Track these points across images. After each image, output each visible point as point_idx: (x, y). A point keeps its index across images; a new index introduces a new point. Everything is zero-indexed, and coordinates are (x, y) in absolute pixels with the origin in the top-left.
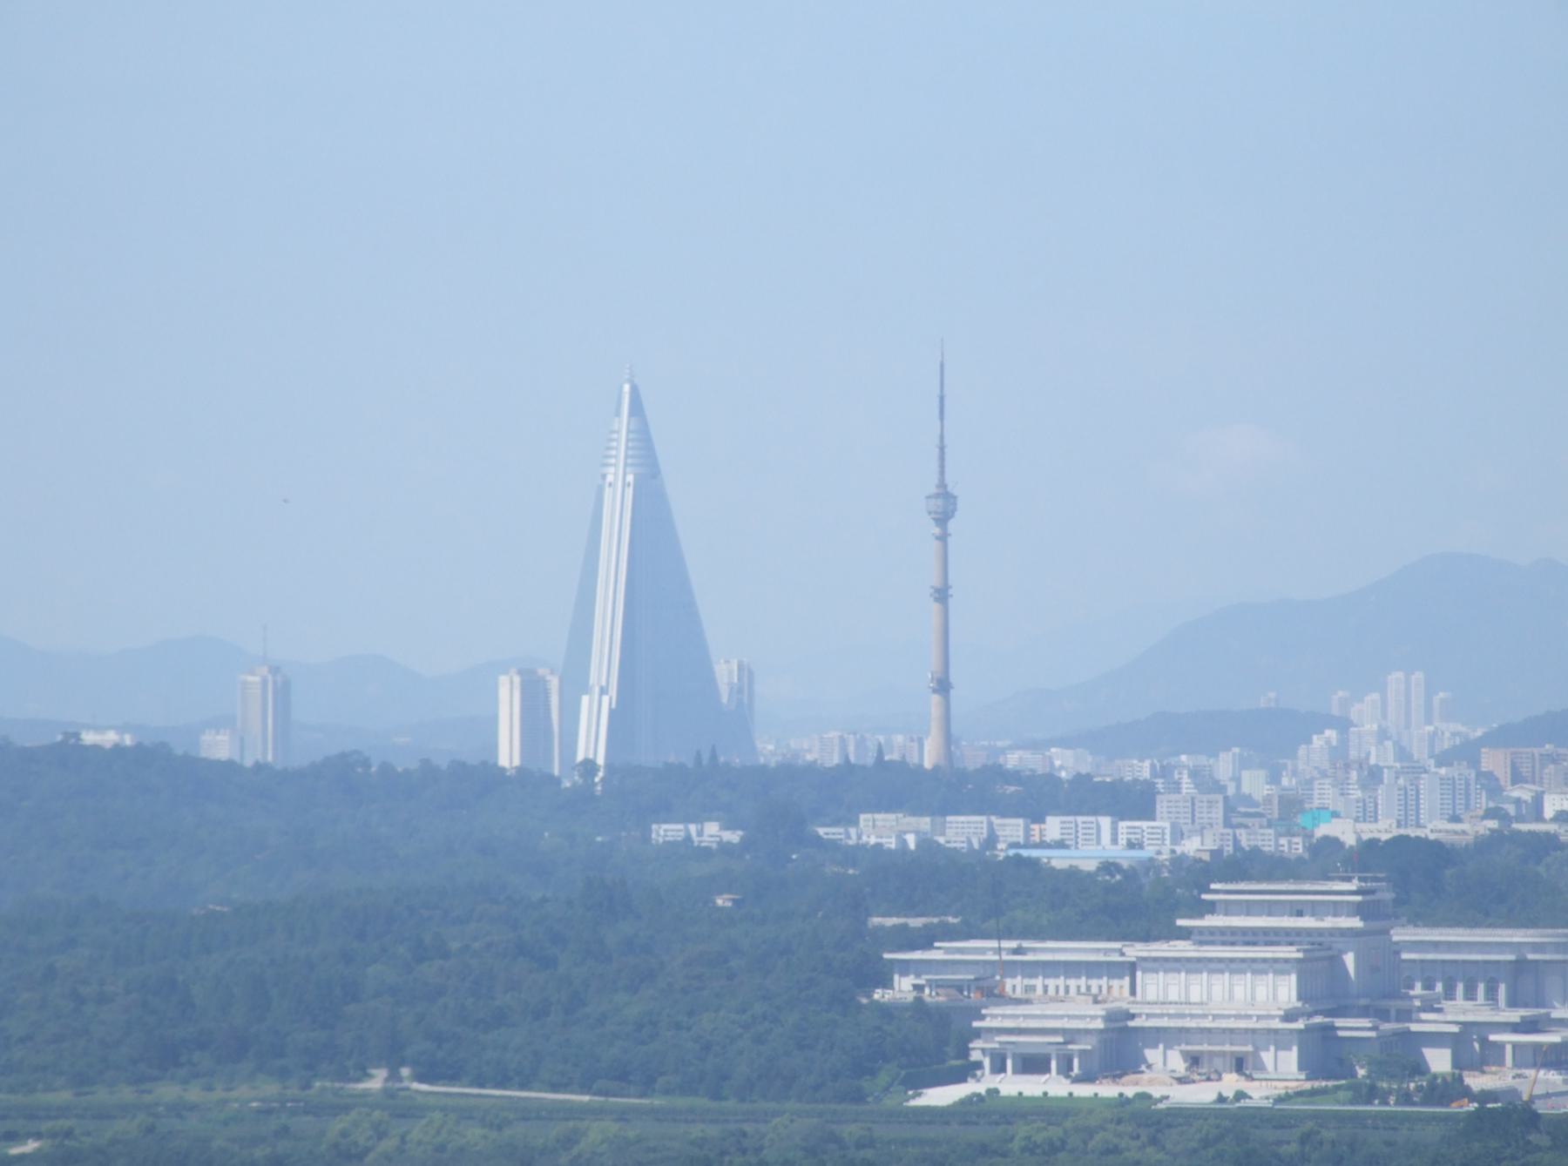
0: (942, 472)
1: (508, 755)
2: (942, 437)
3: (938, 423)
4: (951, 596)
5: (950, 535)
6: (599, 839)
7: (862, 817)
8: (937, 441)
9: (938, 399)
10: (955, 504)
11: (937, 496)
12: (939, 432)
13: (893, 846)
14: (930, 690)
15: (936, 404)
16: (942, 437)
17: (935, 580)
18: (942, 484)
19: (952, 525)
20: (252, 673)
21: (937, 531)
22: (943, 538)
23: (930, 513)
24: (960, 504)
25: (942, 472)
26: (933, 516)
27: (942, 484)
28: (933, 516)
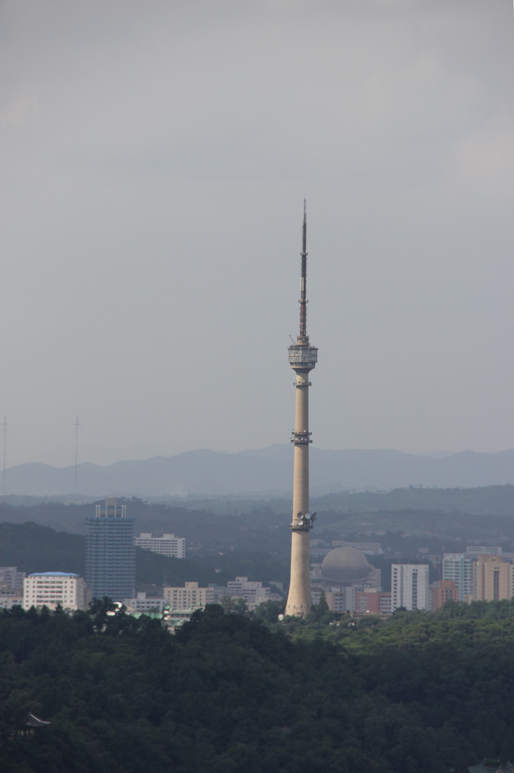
0: (304, 327)
1: (409, 607)
2: (304, 292)
3: (301, 279)
4: (311, 442)
5: (311, 384)
6: (368, 611)
7: (166, 590)
8: (299, 297)
9: (300, 258)
10: (316, 356)
11: (296, 348)
12: (300, 288)
13: (180, 555)
14: (294, 443)
15: (300, 261)
16: (304, 292)
17: (297, 428)
18: (304, 337)
19: (312, 375)
20: (39, 729)
21: (298, 379)
22: (304, 387)
23: (291, 363)
24: (320, 353)
25: (304, 327)
26: (294, 367)
27: (304, 337)
28: (294, 367)
